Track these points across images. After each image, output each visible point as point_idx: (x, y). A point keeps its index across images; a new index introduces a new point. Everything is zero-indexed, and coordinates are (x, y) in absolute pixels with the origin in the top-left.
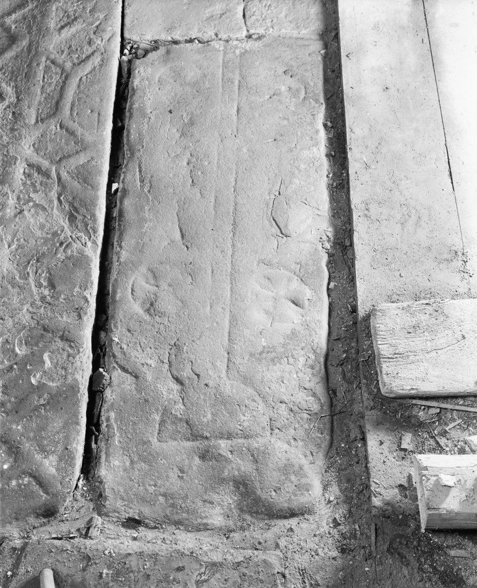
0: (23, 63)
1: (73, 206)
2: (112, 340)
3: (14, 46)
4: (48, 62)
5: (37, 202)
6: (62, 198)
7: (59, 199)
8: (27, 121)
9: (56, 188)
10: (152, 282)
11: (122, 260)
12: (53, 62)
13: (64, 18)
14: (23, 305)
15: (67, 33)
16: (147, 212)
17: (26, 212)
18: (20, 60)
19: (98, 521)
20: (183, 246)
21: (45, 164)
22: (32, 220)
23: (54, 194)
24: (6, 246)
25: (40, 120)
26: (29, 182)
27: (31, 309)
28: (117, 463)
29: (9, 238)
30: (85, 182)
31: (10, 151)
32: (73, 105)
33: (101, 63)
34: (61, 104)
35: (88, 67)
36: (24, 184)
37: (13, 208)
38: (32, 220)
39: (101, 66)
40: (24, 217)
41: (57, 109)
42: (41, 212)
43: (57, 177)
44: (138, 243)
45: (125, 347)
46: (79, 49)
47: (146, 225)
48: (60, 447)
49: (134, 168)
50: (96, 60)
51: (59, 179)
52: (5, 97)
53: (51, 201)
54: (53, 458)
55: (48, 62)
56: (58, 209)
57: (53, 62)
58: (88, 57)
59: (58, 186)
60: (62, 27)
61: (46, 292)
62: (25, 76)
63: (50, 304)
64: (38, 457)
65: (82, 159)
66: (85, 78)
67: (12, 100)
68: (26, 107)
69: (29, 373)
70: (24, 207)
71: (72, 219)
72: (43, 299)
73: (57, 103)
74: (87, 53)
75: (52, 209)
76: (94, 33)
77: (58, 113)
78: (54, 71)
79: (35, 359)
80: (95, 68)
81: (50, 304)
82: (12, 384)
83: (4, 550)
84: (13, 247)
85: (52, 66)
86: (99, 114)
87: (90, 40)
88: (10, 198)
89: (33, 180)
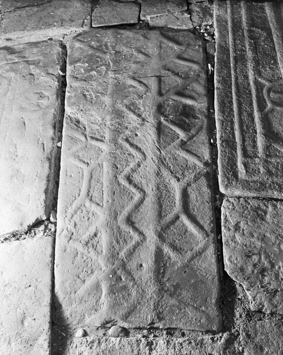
0: (118, 202)
1: (77, 126)
2: (58, 82)
3: (127, 214)
4: (101, 205)
5: (96, 125)
6: (84, 129)
7: (85, 128)
8: (108, 163)
9: (87, 133)
10: (40, 104)
11: (54, 109)
12: (98, 204)
13: (96, 245)
14: (96, 87)
15: (92, 230)
16: (41, 129)
17: (100, 119)
18: (121, 204)
19: (62, 39)
20: (24, 118)
21: (94, 143)
22: (97, 117)
23: (88, 129)
24: (107, 105)
25: (100, 166)
26: (102, 134)
27: (93, 87)
28: (55, 51)
29: (106, 108)
30: (72, 137)
31: (114, 146)
32: (82, 178)
33: (67, 210)
34: (89, 177)
35: (74, 206)
36: (104, 132)
37: (107, 120)
38: (97, 117)
39: (67, 207)
40: (101, 117)
41: (91, 173)
42: (93, 121)
43: (87, 138)
44: (45, 116)
45: (53, 81)
46: (82, 218)
47: (41, 123)
48: (74, 49)
49: (47, 150)
50: (70, 211)
51: (86, 137)
52: (125, 178)
53: (89, 127)
54: (76, 46)
55: (101, 205)
56: (85, 124)
57: (98, 204)
58: (76, 212)
59: (86, 134)
60: (95, 235)
61: (87, 93)
62: (114, 192)
63: (85, 90)
64: (82, 46)
65: (74, 149)
66: (77, 197)
67: (120, 176)
68: (110, 172)
69: (89, 66)
70: (102, 122)
71: (78, 122)
72: (88, 91)
73: (91, 177)
74: (77, 216)
75: (88, 123)
76: (73, 234)
77: (90, 171)
78: (97, 199)
79: (87, 71)
80: (71, 205)
81: (85, 90)
82: (95, 63)
83: (164, 217)
84: (104, 105)
85: (98, 202)
86: (67, 175)
87: (75, 227)
88: (109, 124)
89: (100, 135)
